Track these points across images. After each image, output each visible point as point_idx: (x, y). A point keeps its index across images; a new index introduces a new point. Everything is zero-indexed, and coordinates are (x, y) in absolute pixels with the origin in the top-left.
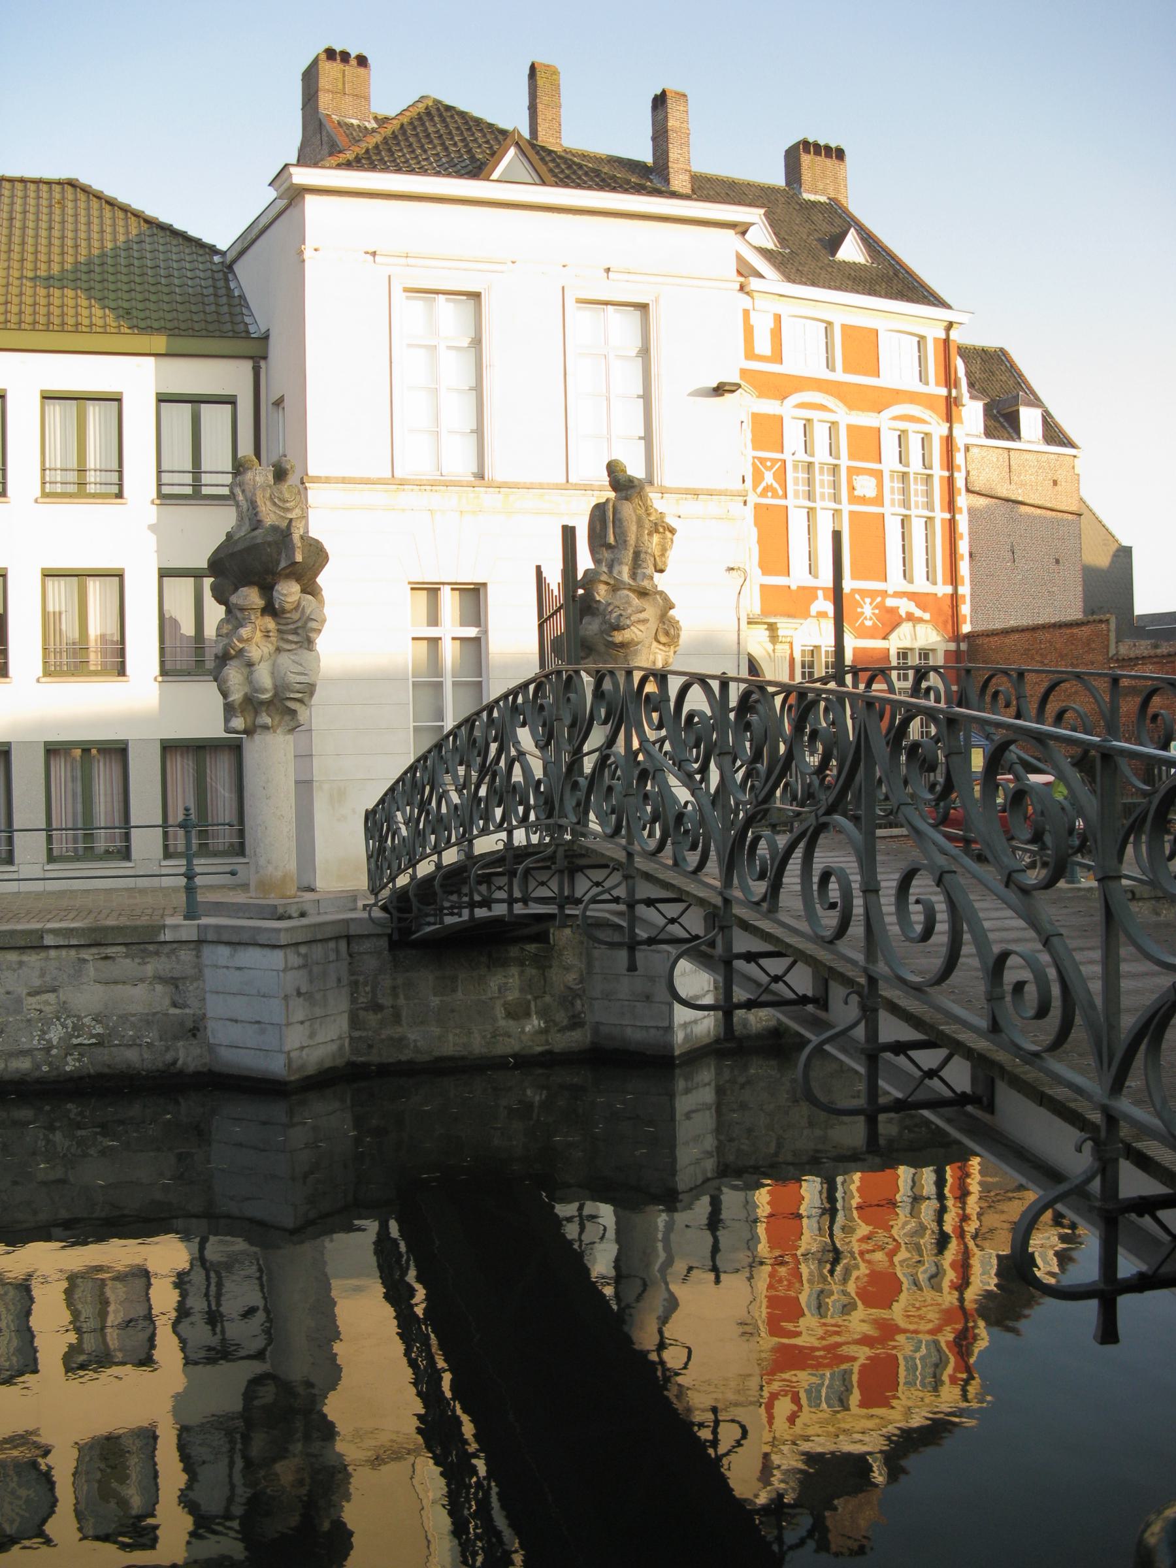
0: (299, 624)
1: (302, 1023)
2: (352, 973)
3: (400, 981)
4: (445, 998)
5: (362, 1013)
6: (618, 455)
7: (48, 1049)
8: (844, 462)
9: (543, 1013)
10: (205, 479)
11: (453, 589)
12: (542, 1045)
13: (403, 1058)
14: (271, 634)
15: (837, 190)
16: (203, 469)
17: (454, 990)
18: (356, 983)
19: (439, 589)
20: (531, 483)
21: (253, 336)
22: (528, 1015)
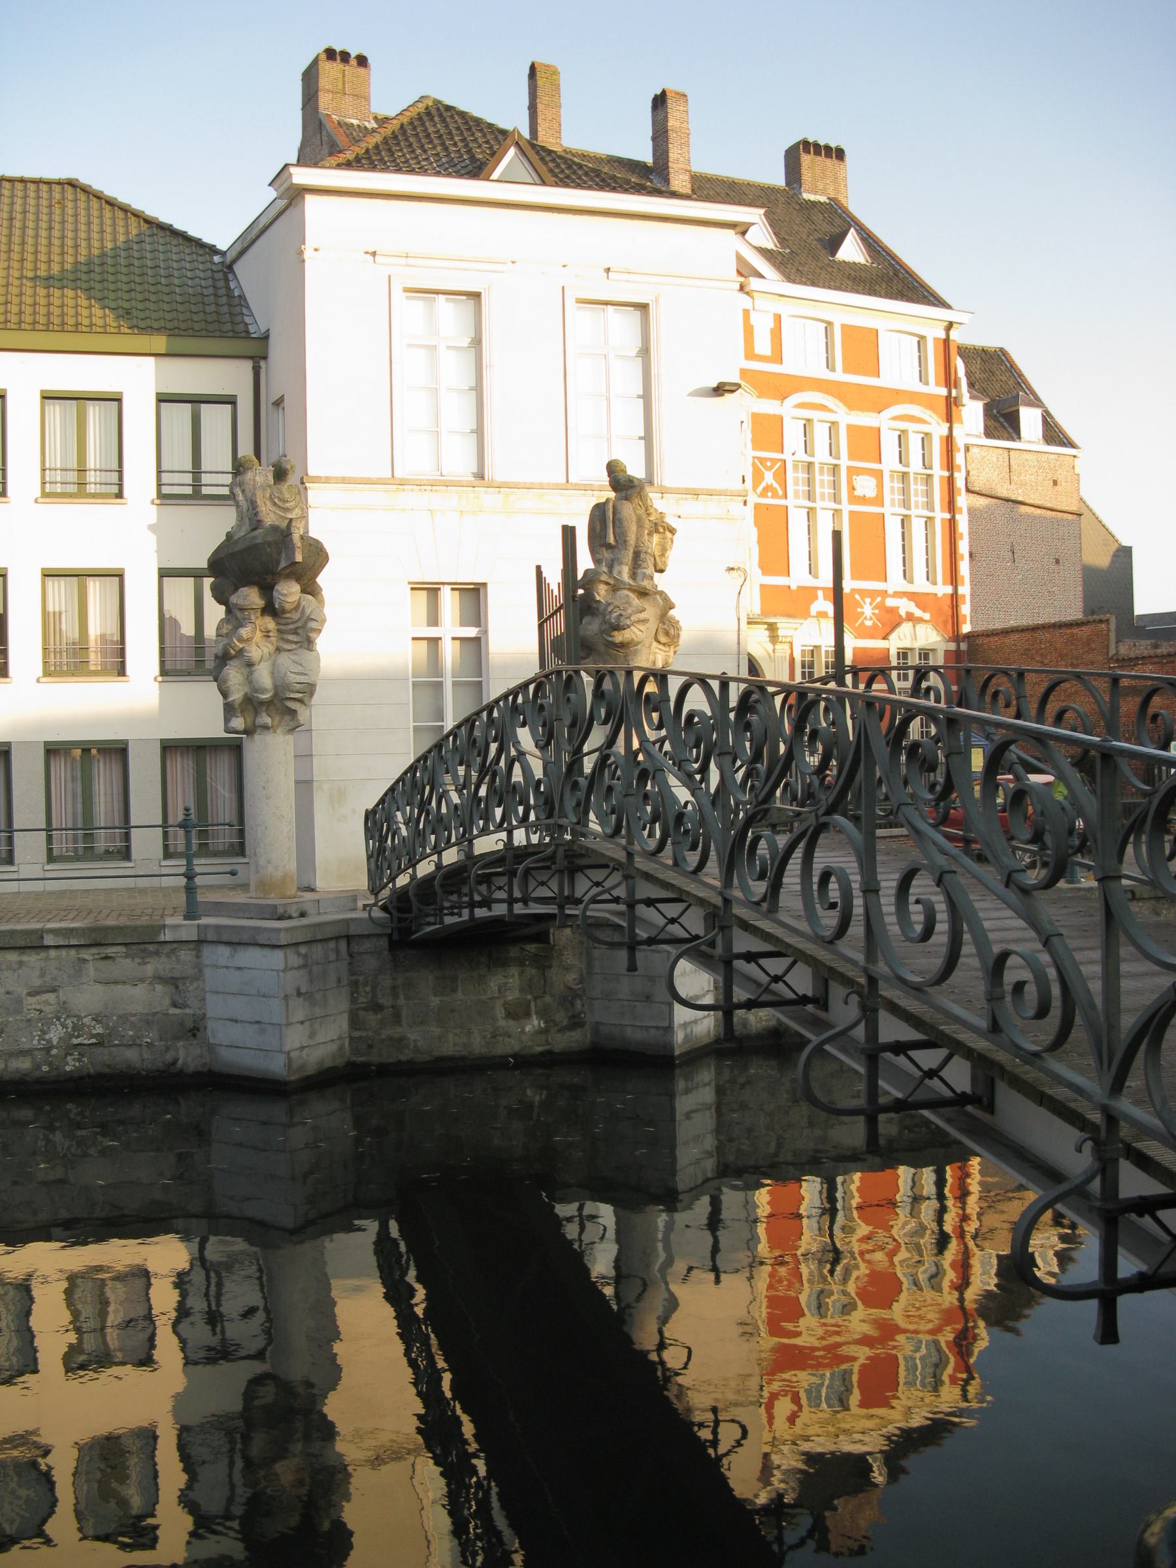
0: (299, 624)
1: (302, 1023)
2: (352, 973)
3: (400, 981)
4: (445, 998)
5: (362, 1013)
6: (618, 455)
7: (48, 1049)
8: (844, 462)
9: (543, 1013)
10: (205, 479)
11: (453, 589)
12: (542, 1045)
13: (403, 1058)
14: (271, 634)
15: (837, 190)
16: (203, 469)
17: (454, 990)
18: (356, 983)
19: (439, 589)
20: (531, 483)
21: (253, 336)
22: (528, 1015)
